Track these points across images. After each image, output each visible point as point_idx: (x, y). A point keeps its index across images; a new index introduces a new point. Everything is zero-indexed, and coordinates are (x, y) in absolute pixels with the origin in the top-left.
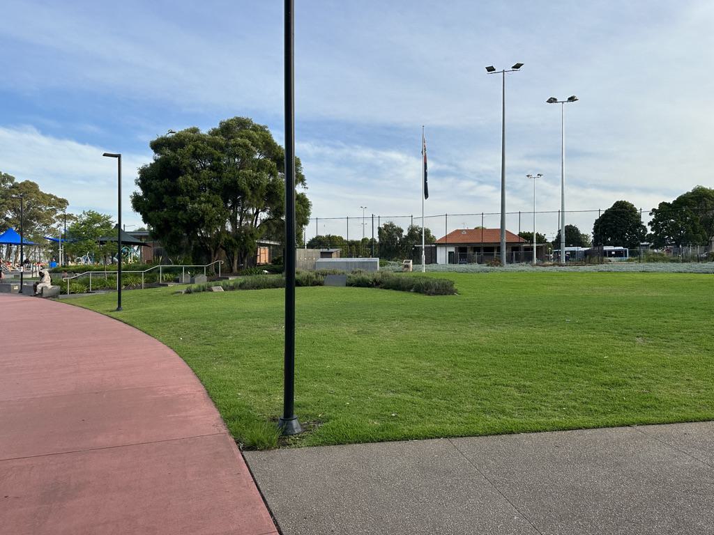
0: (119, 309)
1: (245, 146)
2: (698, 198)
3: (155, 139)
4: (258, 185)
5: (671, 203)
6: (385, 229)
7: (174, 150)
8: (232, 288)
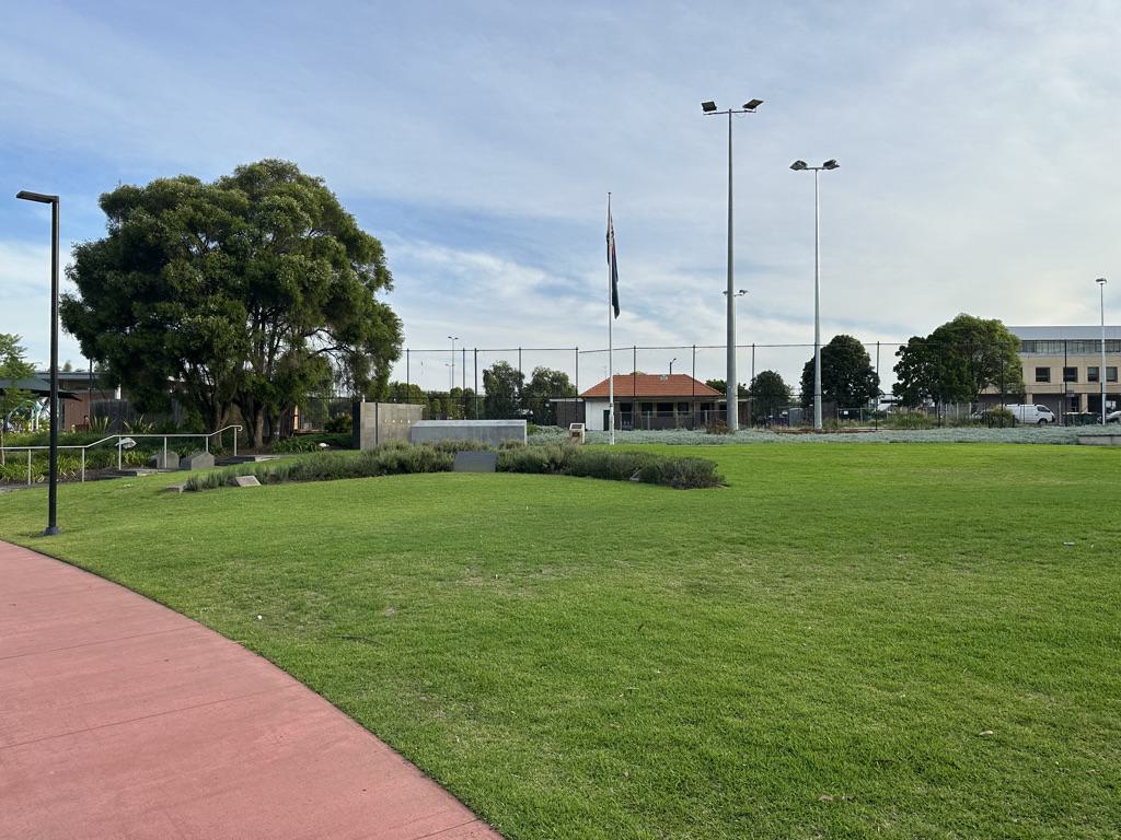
0: (51, 530)
1: (290, 210)
3: (111, 191)
4: (316, 284)
5: (926, 337)
6: (494, 374)
7: (153, 211)
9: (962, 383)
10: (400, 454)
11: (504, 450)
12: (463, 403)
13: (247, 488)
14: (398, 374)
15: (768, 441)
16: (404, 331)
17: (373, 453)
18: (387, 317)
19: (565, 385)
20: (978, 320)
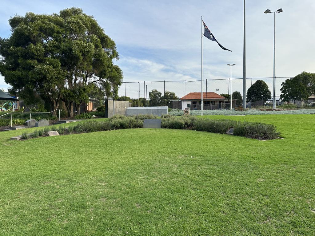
2: (304, 78)
6: (152, 93)
8: (67, 132)
9: (304, 94)
10: (121, 121)
11: (164, 119)
12: (143, 102)
13: (52, 137)
14: (121, 93)
15: (262, 114)
16: (124, 75)
17: (110, 120)
18: (117, 69)
19: (174, 96)
20: (309, 73)
